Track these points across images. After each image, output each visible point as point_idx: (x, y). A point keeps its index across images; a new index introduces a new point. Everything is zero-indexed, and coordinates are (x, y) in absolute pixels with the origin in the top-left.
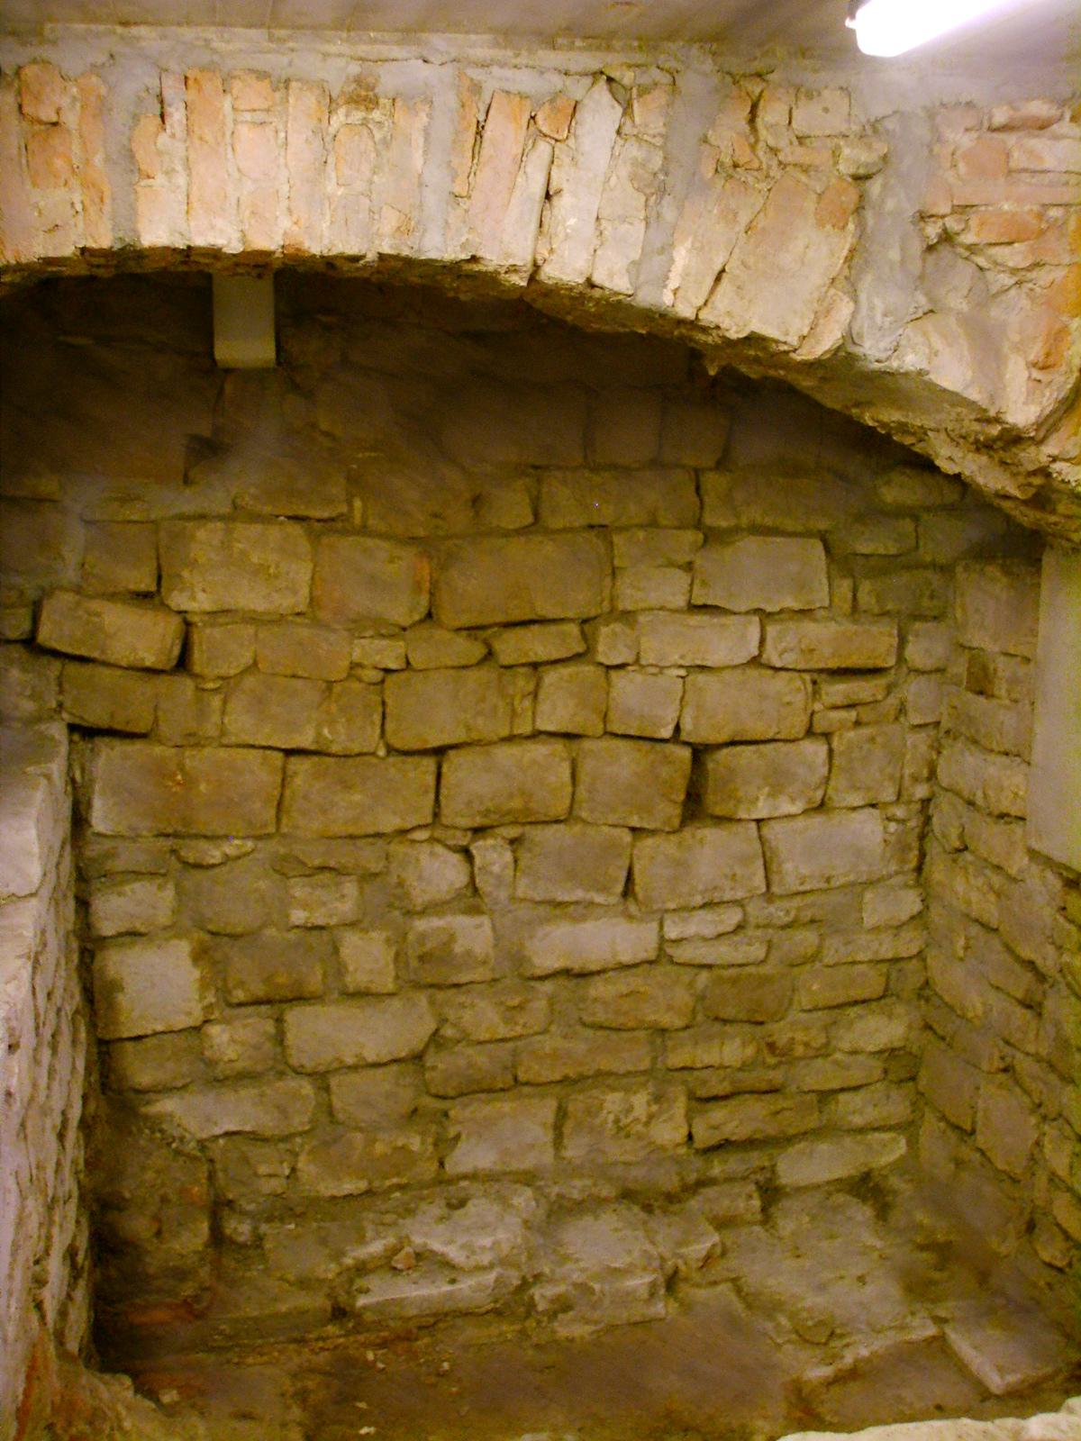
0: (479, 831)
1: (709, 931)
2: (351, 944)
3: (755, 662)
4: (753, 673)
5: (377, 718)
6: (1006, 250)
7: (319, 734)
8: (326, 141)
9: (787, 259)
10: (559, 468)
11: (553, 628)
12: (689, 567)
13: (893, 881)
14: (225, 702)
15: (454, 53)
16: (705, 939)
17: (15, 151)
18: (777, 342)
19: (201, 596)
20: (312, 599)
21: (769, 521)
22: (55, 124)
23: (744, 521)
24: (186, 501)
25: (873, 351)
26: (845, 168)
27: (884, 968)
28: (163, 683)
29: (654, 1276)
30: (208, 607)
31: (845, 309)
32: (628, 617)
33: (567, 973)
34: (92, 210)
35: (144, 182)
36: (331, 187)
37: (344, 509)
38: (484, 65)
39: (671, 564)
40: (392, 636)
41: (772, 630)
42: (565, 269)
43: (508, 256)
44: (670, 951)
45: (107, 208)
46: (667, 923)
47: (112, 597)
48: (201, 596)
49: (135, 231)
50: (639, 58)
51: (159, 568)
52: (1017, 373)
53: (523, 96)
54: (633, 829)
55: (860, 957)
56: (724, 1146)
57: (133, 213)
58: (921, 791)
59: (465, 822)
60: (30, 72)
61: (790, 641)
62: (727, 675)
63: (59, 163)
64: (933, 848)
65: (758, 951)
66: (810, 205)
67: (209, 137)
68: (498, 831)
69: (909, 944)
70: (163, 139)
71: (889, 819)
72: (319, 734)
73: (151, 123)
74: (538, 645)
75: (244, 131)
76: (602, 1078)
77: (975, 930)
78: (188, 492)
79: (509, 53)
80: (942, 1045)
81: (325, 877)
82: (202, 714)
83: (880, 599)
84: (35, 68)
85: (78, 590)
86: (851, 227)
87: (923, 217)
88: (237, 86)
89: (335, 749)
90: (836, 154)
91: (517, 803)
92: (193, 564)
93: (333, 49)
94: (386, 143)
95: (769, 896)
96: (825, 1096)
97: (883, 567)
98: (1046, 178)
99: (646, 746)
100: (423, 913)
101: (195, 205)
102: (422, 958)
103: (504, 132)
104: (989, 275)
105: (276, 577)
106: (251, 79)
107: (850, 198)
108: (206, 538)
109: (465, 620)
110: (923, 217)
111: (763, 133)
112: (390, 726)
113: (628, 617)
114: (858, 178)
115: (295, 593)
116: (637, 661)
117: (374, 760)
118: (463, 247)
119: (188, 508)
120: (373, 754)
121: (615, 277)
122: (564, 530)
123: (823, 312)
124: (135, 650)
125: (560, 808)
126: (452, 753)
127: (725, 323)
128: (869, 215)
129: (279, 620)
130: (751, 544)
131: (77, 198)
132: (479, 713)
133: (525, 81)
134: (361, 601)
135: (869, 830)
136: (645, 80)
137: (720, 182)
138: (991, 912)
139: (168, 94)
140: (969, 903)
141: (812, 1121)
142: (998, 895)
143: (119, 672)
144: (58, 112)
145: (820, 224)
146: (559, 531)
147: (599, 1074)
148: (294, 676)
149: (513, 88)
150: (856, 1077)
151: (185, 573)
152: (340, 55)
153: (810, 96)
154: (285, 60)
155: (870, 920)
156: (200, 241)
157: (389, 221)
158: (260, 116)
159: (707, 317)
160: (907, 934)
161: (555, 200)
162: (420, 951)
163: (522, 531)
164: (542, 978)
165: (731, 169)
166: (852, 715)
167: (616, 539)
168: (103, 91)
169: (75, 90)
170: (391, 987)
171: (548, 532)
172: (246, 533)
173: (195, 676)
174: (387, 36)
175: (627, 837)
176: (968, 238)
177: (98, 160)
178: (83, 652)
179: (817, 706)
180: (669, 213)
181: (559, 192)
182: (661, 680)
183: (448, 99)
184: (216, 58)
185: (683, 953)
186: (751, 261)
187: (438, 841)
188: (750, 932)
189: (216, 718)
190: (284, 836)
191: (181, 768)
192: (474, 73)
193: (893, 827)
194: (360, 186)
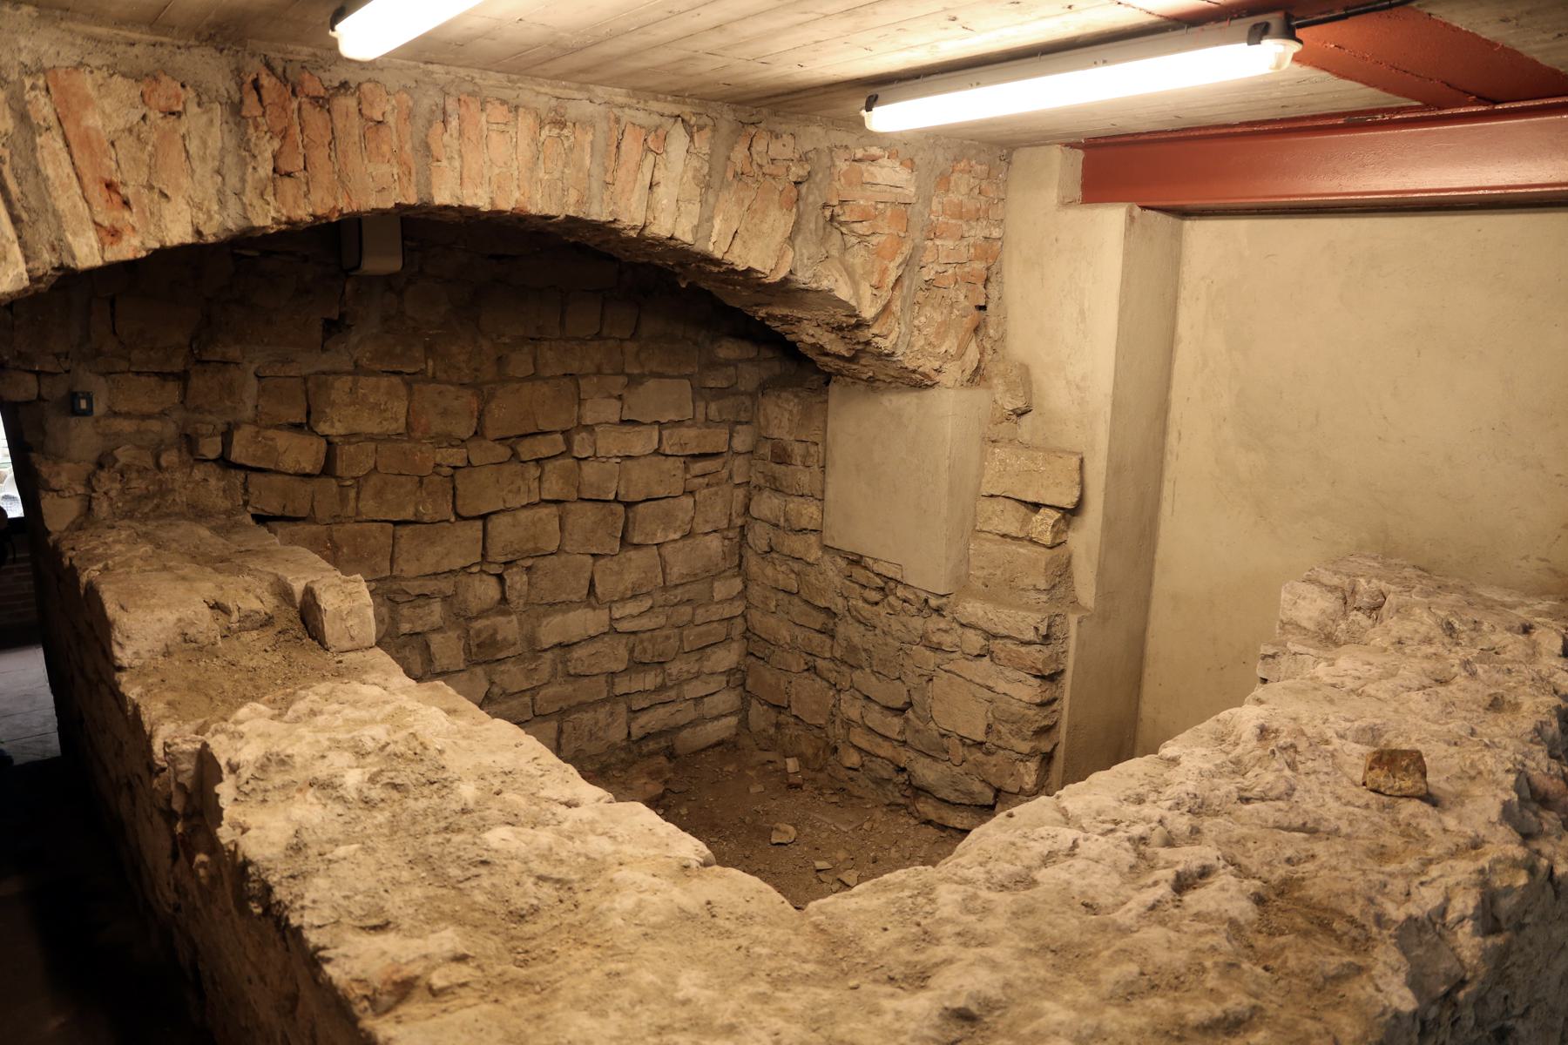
0: (508, 564)
1: (635, 611)
2: (436, 640)
3: (657, 452)
4: (655, 459)
5: (449, 498)
6: (859, 225)
7: (417, 510)
8: (538, 147)
9: (765, 227)
10: (546, 340)
11: (549, 437)
12: (620, 398)
13: (727, 574)
14: (358, 493)
15: (607, 98)
16: (633, 617)
17: (357, 139)
18: (758, 272)
19: (338, 425)
20: (407, 423)
21: (660, 370)
22: (379, 122)
23: (646, 371)
24: (325, 362)
25: (803, 278)
26: (792, 178)
27: (725, 623)
28: (317, 483)
29: (1327, 604)
30: (342, 432)
31: (790, 254)
32: (590, 429)
33: (560, 645)
34: (405, 180)
35: (436, 164)
36: (541, 174)
37: (423, 366)
38: (622, 107)
39: (610, 396)
40: (457, 446)
41: (666, 433)
42: (662, 227)
43: (633, 220)
44: (616, 626)
45: (413, 178)
46: (614, 609)
47: (278, 427)
48: (338, 425)
49: (430, 194)
50: (699, 110)
51: (309, 407)
52: (866, 291)
53: (641, 127)
54: (593, 555)
55: (714, 618)
56: (647, 736)
57: (429, 184)
58: (739, 522)
59: (503, 559)
60: (366, 87)
61: (675, 439)
62: (642, 461)
63: (385, 148)
64: (749, 554)
65: (662, 620)
66: (776, 197)
67: (473, 138)
68: (519, 562)
69: (738, 608)
70: (446, 137)
71: (725, 538)
72: (417, 510)
73: (438, 126)
74: (543, 447)
75: (494, 135)
76: (582, 706)
77: (781, 595)
78: (324, 356)
79: (635, 101)
80: (762, 662)
81: (421, 602)
82: (343, 500)
83: (720, 412)
84: (370, 85)
85: (255, 423)
86: (794, 210)
87: (825, 206)
88: (489, 106)
89: (426, 519)
90: (788, 169)
91: (530, 545)
92: (333, 404)
93: (543, 90)
94: (571, 149)
95: (665, 588)
96: (698, 700)
97: (720, 393)
98: (877, 188)
99: (600, 505)
100: (476, 618)
101: (466, 180)
102: (479, 646)
103: (631, 147)
104: (846, 238)
105: (385, 411)
106: (497, 103)
107: (794, 194)
108: (341, 386)
109: (498, 435)
110: (825, 206)
111: (755, 156)
112: (459, 503)
113: (590, 429)
114: (797, 183)
115: (397, 420)
116: (595, 455)
117: (447, 524)
118: (611, 213)
119: (325, 367)
120: (448, 521)
121: (685, 234)
122: (552, 377)
123: (781, 257)
124: (299, 462)
125: (553, 548)
126: (493, 517)
127: (737, 261)
128: (801, 203)
129: (387, 438)
130: (651, 383)
131: (395, 171)
132: (510, 491)
133: (641, 117)
134: (438, 425)
135: (714, 544)
136: (701, 122)
137: (735, 183)
138: (793, 585)
139: (449, 108)
140: (776, 581)
141: (692, 715)
142: (798, 574)
143: (287, 478)
144: (383, 114)
145: (781, 208)
146: (549, 378)
147: (580, 704)
148: (400, 474)
149: (637, 122)
150: (712, 688)
151: (328, 410)
152: (546, 94)
153: (777, 138)
154: (514, 94)
155: (717, 597)
156: (468, 203)
157: (573, 196)
158: (502, 127)
159: (729, 258)
160: (737, 603)
161: (655, 189)
162: (477, 641)
163: (528, 378)
164: (545, 650)
165: (739, 175)
166: (706, 480)
167: (581, 382)
168: (411, 103)
169: (394, 102)
170: (462, 666)
171: (545, 379)
172: (367, 382)
173: (336, 477)
174: (572, 85)
175: (590, 560)
176: (842, 219)
177: (408, 147)
178: (262, 465)
179: (688, 476)
180: (711, 200)
181: (658, 183)
182: (607, 466)
183: (602, 126)
184: (477, 89)
185: (621, 626)
186: (750, 227)
187: (485, 572)
188: (656, 610)
189: (352, 503)
190: (395, 577)
191: (331, 540)
192: (616, 111)
193: (726, 542)
194: (557, 175)
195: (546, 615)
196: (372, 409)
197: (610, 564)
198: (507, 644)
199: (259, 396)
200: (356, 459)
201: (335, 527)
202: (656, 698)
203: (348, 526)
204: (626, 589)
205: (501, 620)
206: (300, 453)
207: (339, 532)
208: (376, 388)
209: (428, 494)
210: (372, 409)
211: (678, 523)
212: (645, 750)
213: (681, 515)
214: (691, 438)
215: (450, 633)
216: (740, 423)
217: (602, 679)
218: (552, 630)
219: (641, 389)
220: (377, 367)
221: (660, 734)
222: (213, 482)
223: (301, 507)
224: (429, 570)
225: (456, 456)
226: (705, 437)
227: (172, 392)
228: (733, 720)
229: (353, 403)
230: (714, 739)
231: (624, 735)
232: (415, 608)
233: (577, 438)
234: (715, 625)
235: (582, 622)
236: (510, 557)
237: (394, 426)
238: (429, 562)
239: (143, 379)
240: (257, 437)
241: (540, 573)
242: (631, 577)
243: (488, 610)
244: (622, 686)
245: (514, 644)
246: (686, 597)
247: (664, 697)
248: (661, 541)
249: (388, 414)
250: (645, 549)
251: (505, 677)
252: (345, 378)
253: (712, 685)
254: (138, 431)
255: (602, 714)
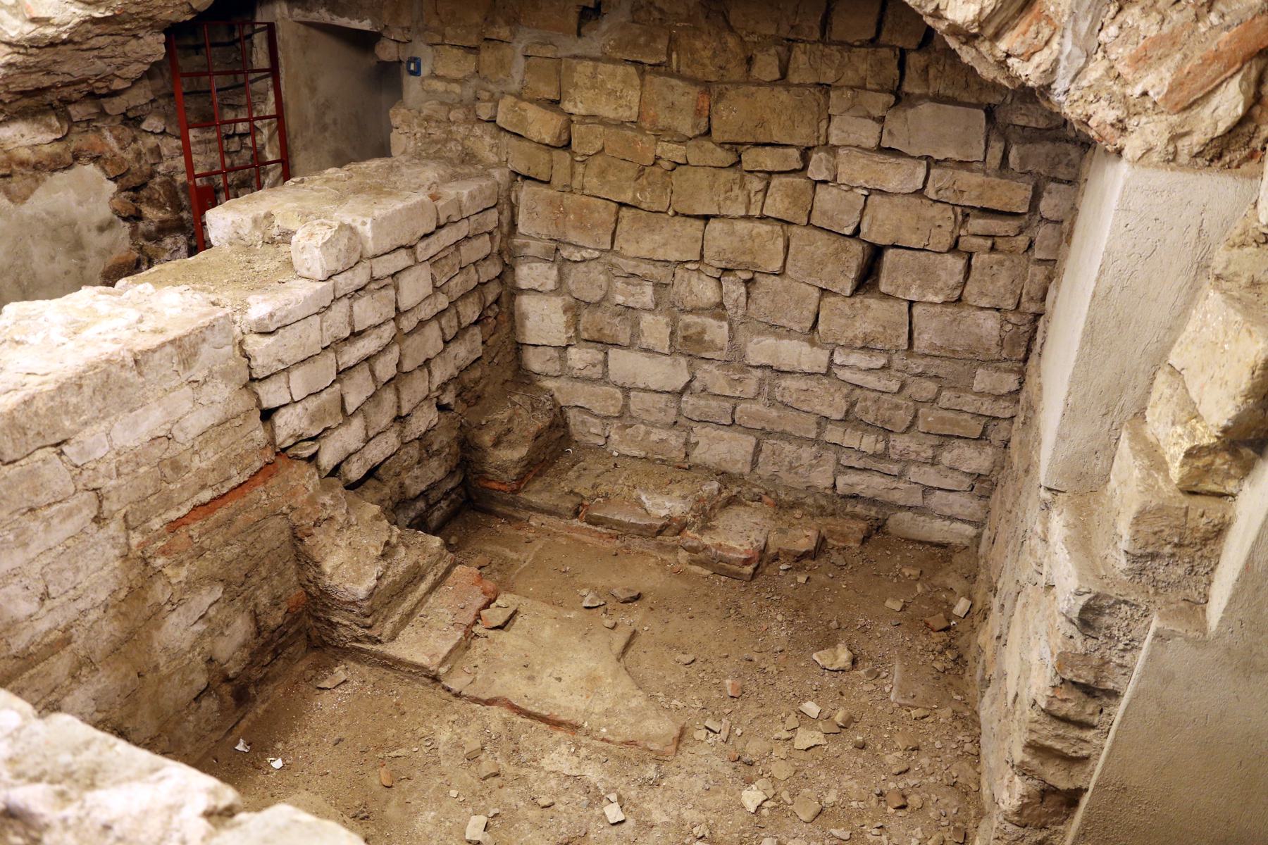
1: (863, 365)
2: (647, 320)
3: (920, 193)
4: (915, 201)
7: (635, 196)
12: (881, 120)
19: (580, 105)
21: (949, 93)
24: (579, 47)
30: (583, 112)
32: (832, 150)
46: (836, 353)
47: (531, 101)
48: (580, 105)
61: (945, 182)
62: (896, 200)
72: (635, 196)
74: (768, 159)
76: (784, 436)
78: (580, 41)
89: (644, 206)
92: (576, 86)
99: (833, 237)
102: (685, 338)
109: (726, 138)
113: (832, 150)
119: (577, 51)
124: (540, 133)
129: (621, 124)
134: (664, 120)
135: (989, 324)
141: (917, 500)
150: (948, 483)
151: (571, 91)
155: (977, 386)
163: (773, 83)
195: (760, 333)
196: (609, 94)
197: (840, 305)
198: (712, 346)
199: (525, 72)
200: (587, 140)
201: (566, 195)
202: (870, 463)
203: (576, 197)
204: (855, 337)
205: (710, 322)
206: (543, 126)
207: (569, 200)
208: (616, 76)
209: (649, 184)
210: (609, 94)
211: (940, 284)
212: (849, 509)
213: (944, 276)
214: (973, 187)
215: (660, 318)
216: (1055, 180)
217: (813, 419)
218: (761, 349)
219: (910, 113)
220: (619, 55)
221: (872, 501)
222: (487, 139)
223: (542, 172)
224: (643, 254)
225: (672, 151)
226: (993, 188)
227: (469, 64)
228: (970, 530)
229: (594, 87)
230: (937, 538)
231: (829, 483)
232: (628, 284)
233: (815, 157)
234: (966, 417)
235: (796, 353)
236: (729, 266)
237: (627, 114)
238: (644, 249)
239: (455, 51)
240: (514, 107)
241: (762, 290)
242: (862, 327)
243: (703, 309)
244: (833, 434)
245: (721, 349)
246: (933, 372)
247: (883, 466)
248: (915, 298)
249: (623, 102)
250: (891, 302)
251: (707, 376)
252: (586, 63)
253: (949, 481)
254: (446, 91)
255: (807, 453)
